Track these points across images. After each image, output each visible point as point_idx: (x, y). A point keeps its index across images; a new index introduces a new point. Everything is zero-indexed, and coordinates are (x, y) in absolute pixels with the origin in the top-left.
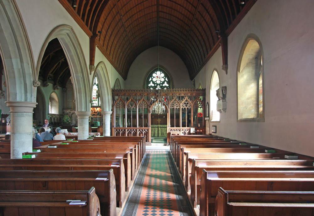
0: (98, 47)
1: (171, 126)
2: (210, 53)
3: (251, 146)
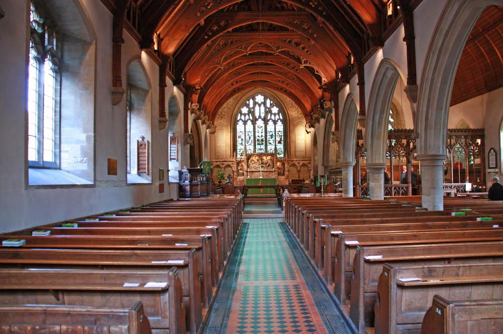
0: (130, 31)
1: (447, 181)
2: (368, 53)
3: (478, 218)
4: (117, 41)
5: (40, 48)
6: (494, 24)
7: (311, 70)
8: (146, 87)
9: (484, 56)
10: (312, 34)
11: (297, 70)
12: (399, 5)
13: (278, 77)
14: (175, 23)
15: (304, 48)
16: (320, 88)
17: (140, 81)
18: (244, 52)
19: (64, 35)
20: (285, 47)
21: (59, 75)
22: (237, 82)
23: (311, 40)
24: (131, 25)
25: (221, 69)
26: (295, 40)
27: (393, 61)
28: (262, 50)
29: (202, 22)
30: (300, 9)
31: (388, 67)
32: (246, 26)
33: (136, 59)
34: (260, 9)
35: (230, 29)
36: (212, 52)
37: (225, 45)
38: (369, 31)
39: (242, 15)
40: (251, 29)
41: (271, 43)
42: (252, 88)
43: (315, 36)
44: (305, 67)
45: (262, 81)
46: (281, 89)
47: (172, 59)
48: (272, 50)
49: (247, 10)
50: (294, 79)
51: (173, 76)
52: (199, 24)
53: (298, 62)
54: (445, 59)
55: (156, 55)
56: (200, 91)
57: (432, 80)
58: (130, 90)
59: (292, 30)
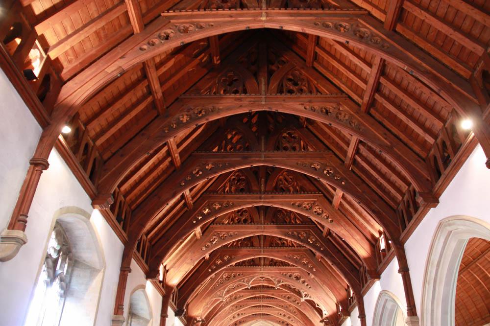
0: (138, 261)
2: (366, 286)
4: (125, 270)
5: (51, 272)
6: (482, 253)
7: (312, 303)
8: (148, 317)
9: (481, 283)
10: (312, 269)
11: (298, 303)
12: (390, 240)
13: (280, 310)
14: (181, 256)
15: (304, 282)
16: (321, 321)
17: (142, 309)
18: (246, 286)
19: (76, 261)
20: (286, 281)
21: (63, 299)
22: (238, 315)
23: (311, 274)
24: (139, 255)
25: (223, 301)
26: (296, 274)
27: (392, 293)
28: (263, 284)
29: (207, 256)
30: (300, 246)
31: (387, 299)
32: (248, 260)
33: (141, 288)
34: (262, 246)
35: (234, 264)
36: (215, 285)
37: (228, 278)
38: (365, 265)
39: (244, 250)
40: (253, 263)
41: (272, 277)
42: (253, 321)
43: (314, 270)
44: (306, 300)
45: (263, 314)
46: (283, 322)
47: (175, 290)
48: (274, 284)
49: (249, 245)
50: (295, 312)
51: (175, 307)
52: (204, 258)
53: (299, 296)
54: (441, 289)
55: (161, 285)
56: (201, 322)
57: (432, 311)
58: (132, 318)
59: (292, 265)
